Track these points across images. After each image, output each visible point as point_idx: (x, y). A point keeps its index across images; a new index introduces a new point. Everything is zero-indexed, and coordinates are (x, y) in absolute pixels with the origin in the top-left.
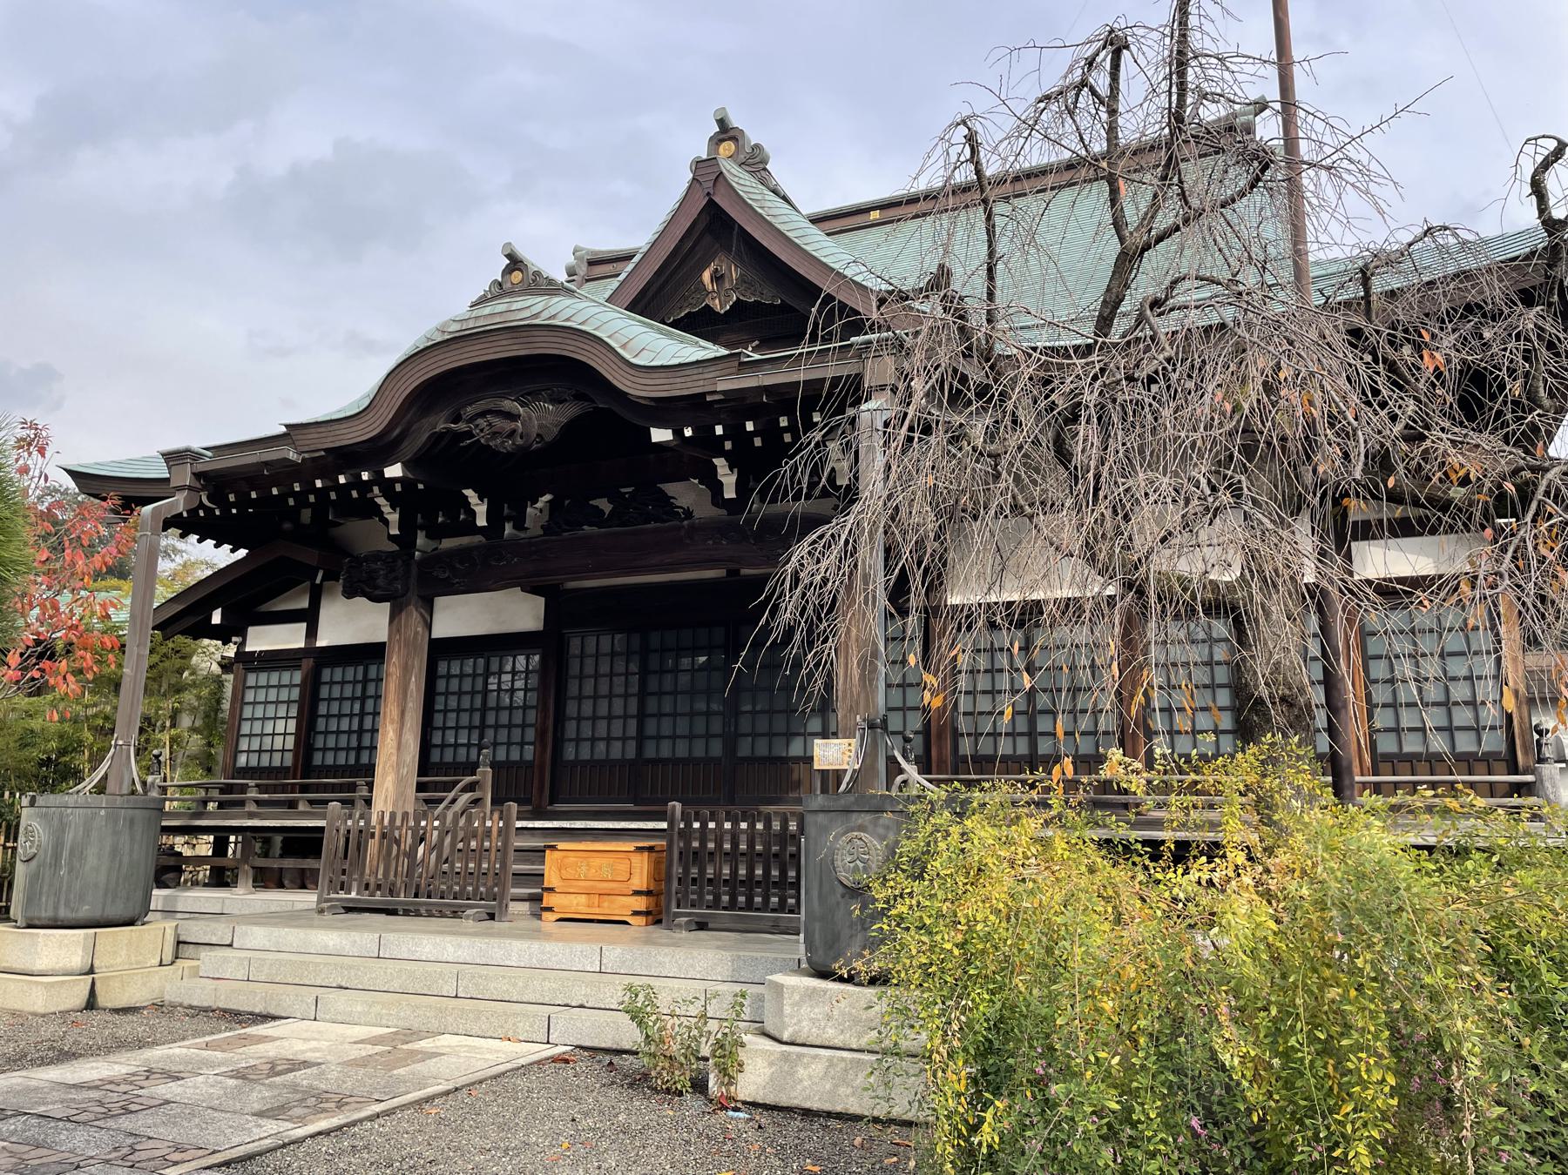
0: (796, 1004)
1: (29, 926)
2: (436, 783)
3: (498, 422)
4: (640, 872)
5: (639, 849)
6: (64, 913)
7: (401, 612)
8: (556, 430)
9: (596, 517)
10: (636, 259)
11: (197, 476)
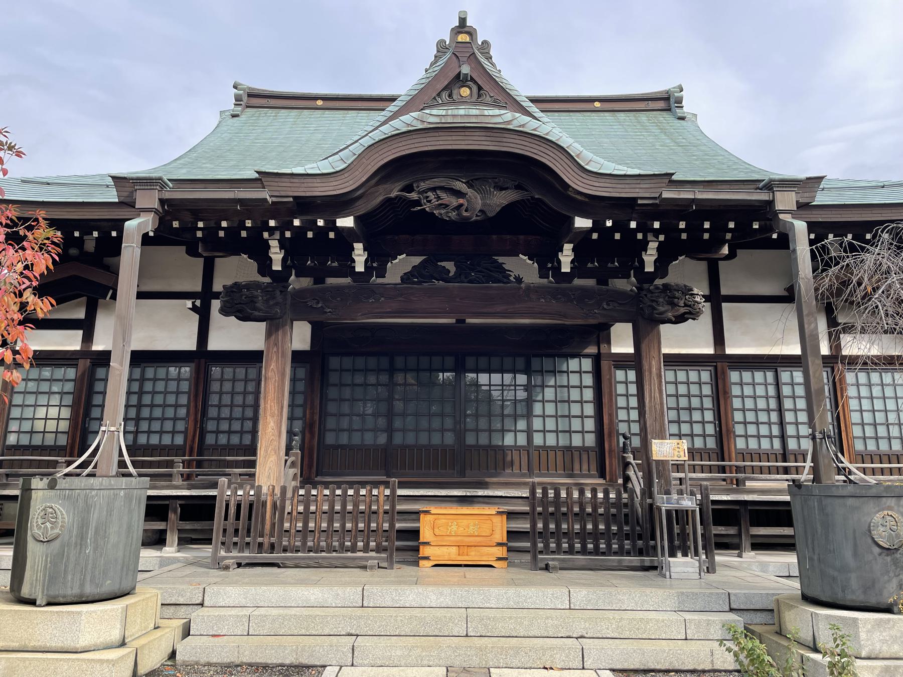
0: (868, 631)
1: (49, 604)
2: (237, 461)
3: (446, 198)
4: (499, 528)
5: (499, 513)
6: (89, 590)
7: (277, 330)
8: (498, 209)
9: (443, 275)
10: (398, 103)
11: (162, 201)
